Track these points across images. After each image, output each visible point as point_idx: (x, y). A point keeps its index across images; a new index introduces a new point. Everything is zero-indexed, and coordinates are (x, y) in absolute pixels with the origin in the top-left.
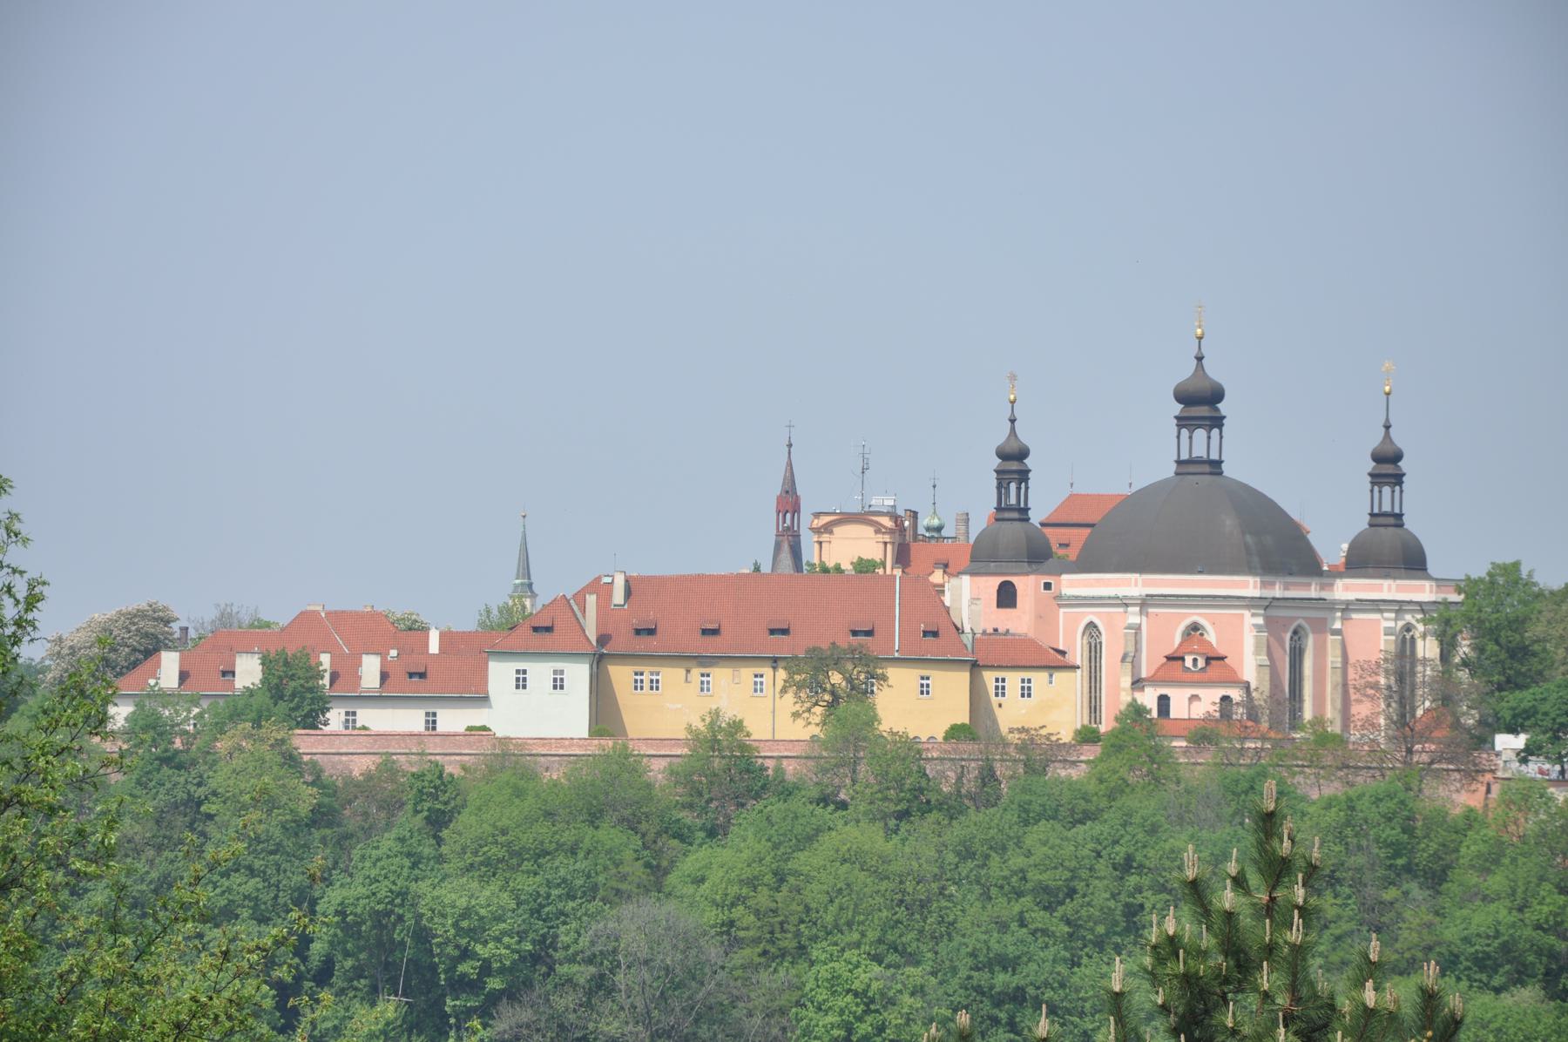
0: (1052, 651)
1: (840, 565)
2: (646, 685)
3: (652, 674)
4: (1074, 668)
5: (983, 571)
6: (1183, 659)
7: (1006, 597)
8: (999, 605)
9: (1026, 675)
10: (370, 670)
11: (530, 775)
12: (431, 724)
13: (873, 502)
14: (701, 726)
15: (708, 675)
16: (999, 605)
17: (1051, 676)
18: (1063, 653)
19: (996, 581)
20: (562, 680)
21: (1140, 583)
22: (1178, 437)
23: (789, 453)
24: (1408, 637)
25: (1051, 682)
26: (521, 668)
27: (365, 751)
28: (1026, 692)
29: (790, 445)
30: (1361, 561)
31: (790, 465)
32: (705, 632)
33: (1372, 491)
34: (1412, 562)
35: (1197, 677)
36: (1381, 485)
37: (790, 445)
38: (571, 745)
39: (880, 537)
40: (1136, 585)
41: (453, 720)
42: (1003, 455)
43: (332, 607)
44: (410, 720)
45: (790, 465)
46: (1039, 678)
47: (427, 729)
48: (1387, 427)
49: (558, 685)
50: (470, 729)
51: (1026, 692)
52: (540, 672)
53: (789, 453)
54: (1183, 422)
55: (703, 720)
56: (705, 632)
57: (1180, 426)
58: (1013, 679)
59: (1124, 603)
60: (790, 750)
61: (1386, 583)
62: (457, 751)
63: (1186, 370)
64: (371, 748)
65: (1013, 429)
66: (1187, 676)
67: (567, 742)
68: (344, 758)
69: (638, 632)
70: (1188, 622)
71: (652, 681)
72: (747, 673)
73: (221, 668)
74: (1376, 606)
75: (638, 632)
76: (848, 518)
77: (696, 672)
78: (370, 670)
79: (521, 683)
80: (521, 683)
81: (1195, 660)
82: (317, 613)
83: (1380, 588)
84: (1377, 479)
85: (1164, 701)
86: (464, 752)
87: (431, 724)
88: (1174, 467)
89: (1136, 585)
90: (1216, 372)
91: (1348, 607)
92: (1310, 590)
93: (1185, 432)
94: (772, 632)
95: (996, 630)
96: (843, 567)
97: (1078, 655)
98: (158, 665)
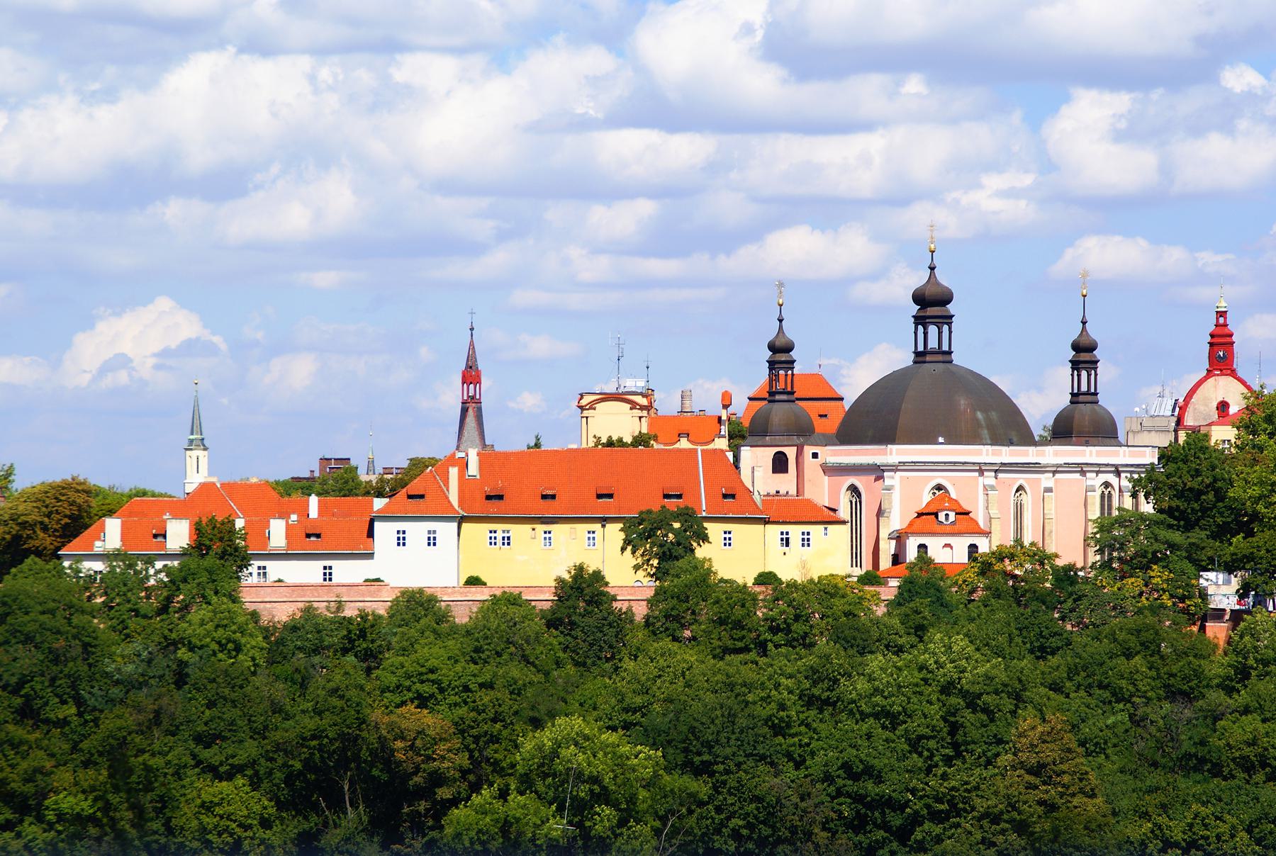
0: (826, 510)
1: (622, 438)
2: (499, 541)
3: (504, 532)
4: (844, 522)
5: (760, 443)
6: (936, 515)
7: (780, 464)
8: (774, 471)
9: (806, 528)
10: (278, 533)
11: (442, 617)
12: (328, 575)
13: (627, 385)
14: (567, 576)
15: (550, 532)
16: (774, 471)
17: (826, 529)
18: (834, 510)
19: (772, 451)
20: (435, 538)
21: (894, 453)
22: (916, 333)
23: (472, 336)
24: (1106, 493)
25: (826, 534)
26: (401, 529)
27: (285, 599)
28: (806, 542)
29: (472, 329)
30: (1063, 431)
31: (472, 344)
32: (544, 497)
33: (1072, 375)
34: (1105, 432)
35: (948, 529)
36: (940, 352)
37: (472, 329)
38: (453, 593)
39: (637, 413)
40: (987, 455)
41: (348, 572)
42: (773, 347)
43: (226, 480)
44: (308, 572)
45: (472, 344)
46: (817, 531)
47: (325, 580)
48: (1084, 323)
49: (432, 542)
50: (366, 581)
51: (806, 542)
52: (417, 531)
53: (472, 336)
54: (920, 320)
55: (570, 572)
56: (544, 497)
57: (916, 324)
58: (795, 532)
59: (981, 469)
60: (631, 595)
61: (1004, 449)
62: (361, 599)
63: (771, 335)
64: (291, 597)
65: (781, 327)
66: (943, 527)
67: (450, 590)
68: (268, 605)
69: (489, 498)
70: (934, 483)
71: (503, 538)
72: (583, 528)
73: (154, 531)
74: (1082, 469)
75: (489, 498)
76: (608, 397)
77: (541, 528)
78: (278, 533)
79: (401, 541)
80: (401, 541)
81: (947, 515)
82: (214, 484)
83: (980, 453)
84: (1076, 365)
85: (923, 547)
86: (366, 599)
87: (328, 575)
88: (913, 356)
89: (891, 454)
90: (945, 279)
91: (895, 468)
92: (1085, 456)
93: (945, 348)
94: (599, 496)
95: (778, 492)
96: (624, 440)
97: (844, 513)
98: (103, 529)
